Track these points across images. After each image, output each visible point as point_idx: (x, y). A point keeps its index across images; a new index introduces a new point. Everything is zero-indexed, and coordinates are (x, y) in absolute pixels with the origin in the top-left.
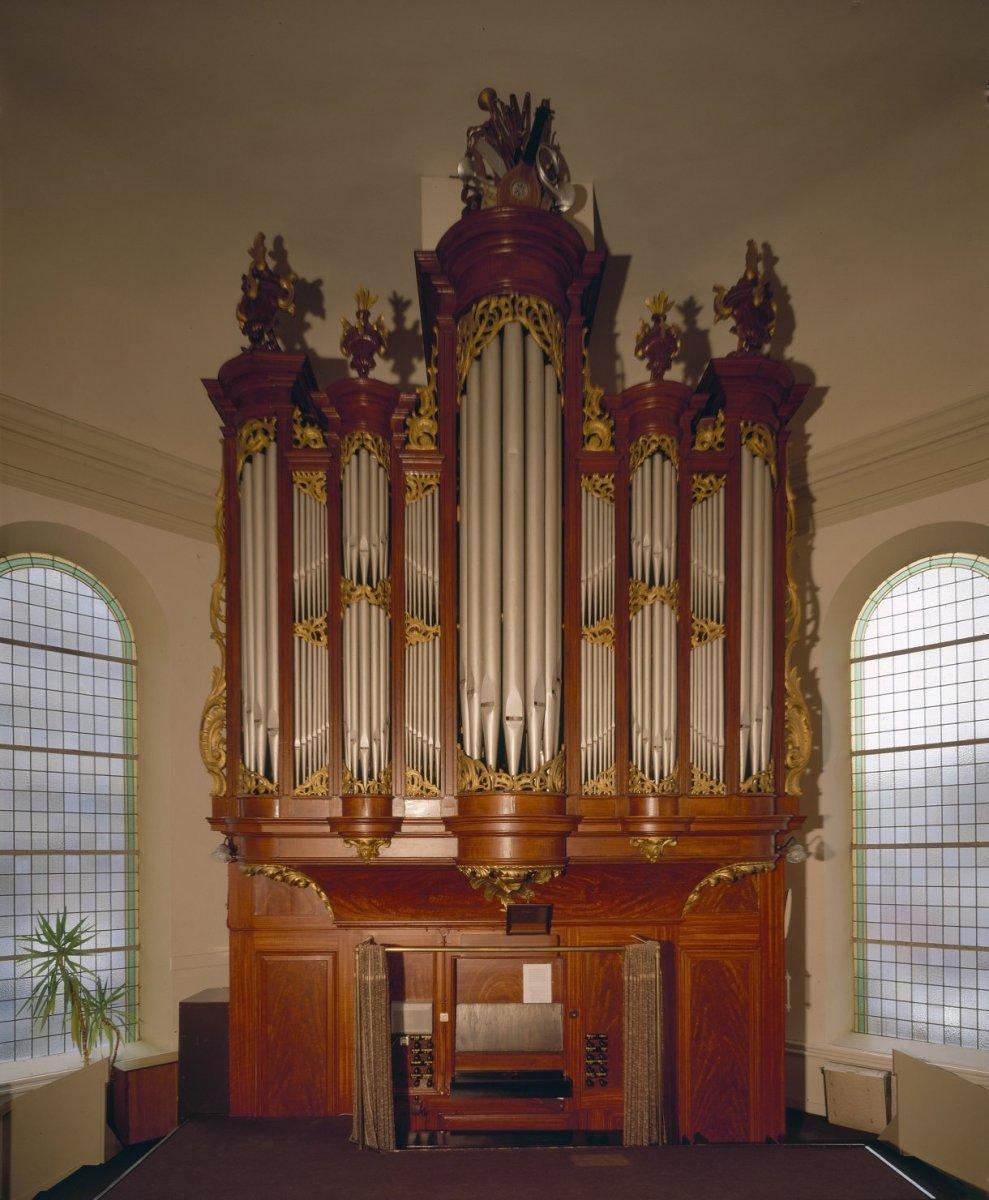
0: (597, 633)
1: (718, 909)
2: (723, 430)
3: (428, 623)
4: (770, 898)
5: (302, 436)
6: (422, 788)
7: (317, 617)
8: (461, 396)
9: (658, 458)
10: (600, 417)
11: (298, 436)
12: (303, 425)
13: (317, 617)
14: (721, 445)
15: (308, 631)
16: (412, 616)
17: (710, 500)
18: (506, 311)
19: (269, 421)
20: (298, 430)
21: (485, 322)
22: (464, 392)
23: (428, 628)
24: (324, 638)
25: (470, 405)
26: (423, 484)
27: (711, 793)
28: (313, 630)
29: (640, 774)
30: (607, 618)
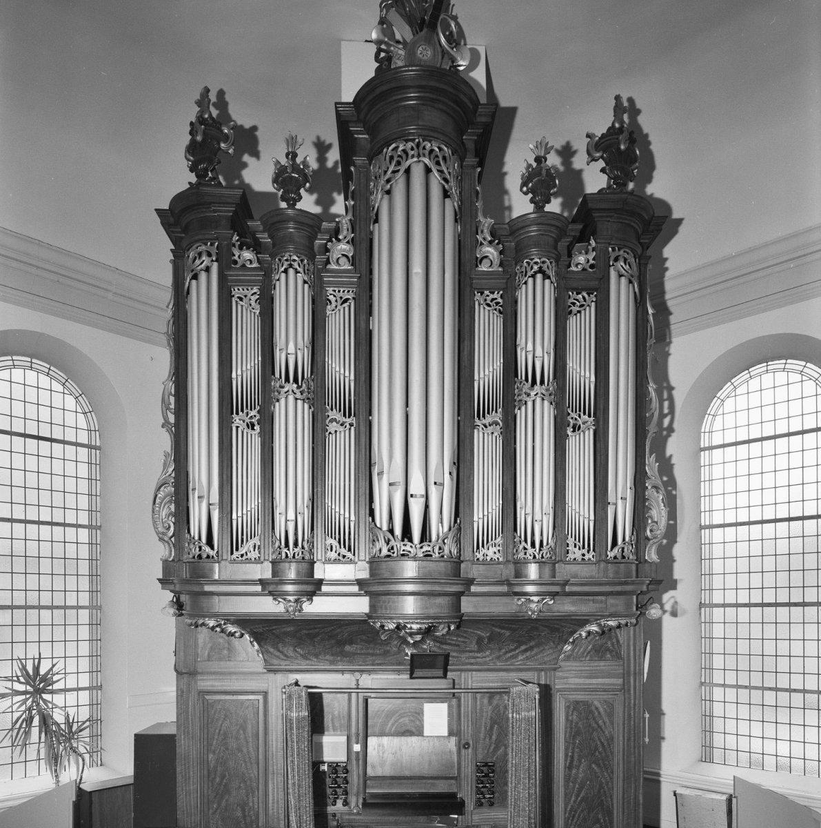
0: (488, 425)
1: (588, 658)
2: (594, 253)
3: (345, 415)
4: (632, 648)
5: (239, 257)
6: (339, 554)
7: (251, 410)
8: (374, 224)
9: (539, 276)
10: (491, 242)
11: (236, 258)
12: (241, 248)
13: (251, 410)
14: (592, 266)
15: (244, 421)
16: (332, 410)
17: (583, 312)
18: (412, 152)
19: (212, 245)
20: (236, 252)
21: (394, 163)
22: (376, 221)
23: (344, 419)
24: (257, 427)
25: (381, 232)
26: (341, 298)
27: (583, 559)
28: (248, 420)
29: (523, 543)
30: (496, 412)
